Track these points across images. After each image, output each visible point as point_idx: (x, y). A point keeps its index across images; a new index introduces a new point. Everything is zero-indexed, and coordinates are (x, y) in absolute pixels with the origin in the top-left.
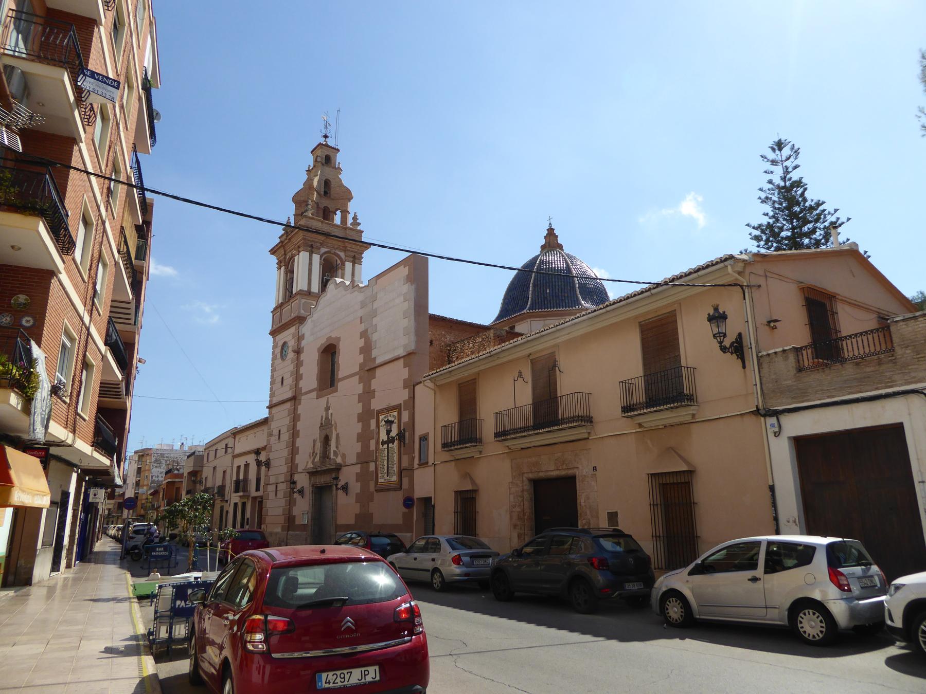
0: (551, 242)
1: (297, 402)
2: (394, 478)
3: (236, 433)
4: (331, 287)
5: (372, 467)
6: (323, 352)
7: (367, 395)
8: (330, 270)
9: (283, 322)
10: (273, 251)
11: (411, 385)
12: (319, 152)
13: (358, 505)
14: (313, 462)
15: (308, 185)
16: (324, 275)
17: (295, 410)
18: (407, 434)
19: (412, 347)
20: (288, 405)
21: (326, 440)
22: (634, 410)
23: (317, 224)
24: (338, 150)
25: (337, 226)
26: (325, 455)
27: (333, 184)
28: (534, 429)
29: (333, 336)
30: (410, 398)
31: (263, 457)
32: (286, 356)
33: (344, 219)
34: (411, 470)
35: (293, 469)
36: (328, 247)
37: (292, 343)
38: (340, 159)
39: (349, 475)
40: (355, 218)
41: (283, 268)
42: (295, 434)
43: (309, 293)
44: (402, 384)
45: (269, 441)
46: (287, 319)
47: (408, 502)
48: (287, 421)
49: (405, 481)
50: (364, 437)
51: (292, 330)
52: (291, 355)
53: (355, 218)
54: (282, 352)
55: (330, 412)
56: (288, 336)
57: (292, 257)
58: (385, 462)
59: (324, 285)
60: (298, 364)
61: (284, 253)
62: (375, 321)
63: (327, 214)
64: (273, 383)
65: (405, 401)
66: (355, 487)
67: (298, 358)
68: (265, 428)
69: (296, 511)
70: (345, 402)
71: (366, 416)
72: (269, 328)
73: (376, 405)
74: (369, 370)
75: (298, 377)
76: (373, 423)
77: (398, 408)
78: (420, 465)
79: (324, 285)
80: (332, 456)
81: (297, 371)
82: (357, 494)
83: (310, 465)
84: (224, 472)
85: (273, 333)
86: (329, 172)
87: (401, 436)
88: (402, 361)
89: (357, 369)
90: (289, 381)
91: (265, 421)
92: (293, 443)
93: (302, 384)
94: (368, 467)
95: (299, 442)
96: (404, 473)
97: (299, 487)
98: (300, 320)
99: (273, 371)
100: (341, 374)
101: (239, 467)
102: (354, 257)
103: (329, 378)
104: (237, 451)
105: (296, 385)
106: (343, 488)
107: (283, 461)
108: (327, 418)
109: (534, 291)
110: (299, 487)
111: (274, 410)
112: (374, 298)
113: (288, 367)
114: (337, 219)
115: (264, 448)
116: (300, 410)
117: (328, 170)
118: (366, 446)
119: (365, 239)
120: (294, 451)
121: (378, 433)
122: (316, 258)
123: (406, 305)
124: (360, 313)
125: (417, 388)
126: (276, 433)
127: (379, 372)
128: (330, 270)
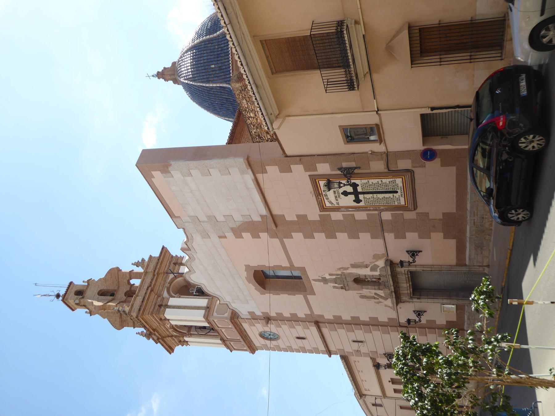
0: (169, 74)
1: (319, 320)
2: (399, 181)
3: (360, 394)
4: (196, 279)
5: (387, 216)
6: (264, 288)
7: (304, 226)
8: (188, 289)
9: (239, 337)
10: (170, 350)
11: (287, 161)
12: (71, 302)
13: (433, 234)
14: (386, 299)
15: (102, 311)
16: (192, 294)
17: (330, 322)
18: (345, 165)
19: (241, 161)
20: (325, 331)
21: (359, 281)
22: (351, 80)
23: (138, 301)
24: (71, 283)
25: (142, 283)
26: (376, 283)
27: (104, 287)
28: (348, 66)
29: (245, 274)
30: (300, 162)
31: (383, 361)
32: (274, 334)
33: (137, 275)
34: (387, 156)
35: (393, 324)
36: (163, 290)
37: (260, 327)
38: (79, 281)
39: (398, 250)
40: (137, 264)
41: (186, 339)
42: (355, 323)
43: (208, 309)
44: (286, 175)
45: (366, 355)
46: (235, 332)
47: (428, 155)
48: (342, 332)
49: (404, 164)
50: (353, 229)
51: (246, 326)
52: (272, 328)
53: (137, 264)
54: (271, 339)
55: (328, 277)
56: (253, 331)
57: (173, 328)
58: (381, 196)
59: (201, 293)
60: (280, 319)
61: (172, 338)
62: (220, 218)
63: (131, 293)
64: (303, 350)
65: (306, 170)
66: (412, 239)
67: (275, 319)
68: (352, 359)
69: (441, 321)
70: (314, 256)
71: (328, 228)
72: (247, 354)
73: (314, 214)
74: (274, 224)
75: (294, 319)
76: (336, 216)
77: (314, 180)
78: (381, 140)
79: (201, 293)
80: (377, 273)
81: (289, 320)
82: (420, 237)
83: (389, 302)
84: (401, 408)
85: (252, 349)
86: (92, 291)
87: (348, 173)
88: (259, 176)
89: (276, 241)
90: (299, 330)
91: (345, 359)
92: (366, 324)
93: (301, 315)
94: (387, 221)
95: (364, 318)
96: (392, 168)
97: (414, 317)
98: (234, 317)
99: (290, 349)
100: (291, 275)
101: (396, 391)
102: (175, 264)
103: (291, 282)
104: (379, 393)
105: (303, 321)
106: (419, 315)
107: (386, 336)
108: (335, 281)
109: (213, 82)
110: (414, 317)
111: (332, 348)
112: (195, 220)
113: (285, 332)
114: (136, 282)
115: (373, 359)
116: (329, 316)
117: (88, 293)
118: (364, 226)
119: (156, 254)
120: (373, 324)
121: (347, 208)
122: (173, 301)
123: (195, 173)
124: (214, 238)
125: (288, 153)
126: (356, 346)
127: (276, 211)
128: (188, 289)
